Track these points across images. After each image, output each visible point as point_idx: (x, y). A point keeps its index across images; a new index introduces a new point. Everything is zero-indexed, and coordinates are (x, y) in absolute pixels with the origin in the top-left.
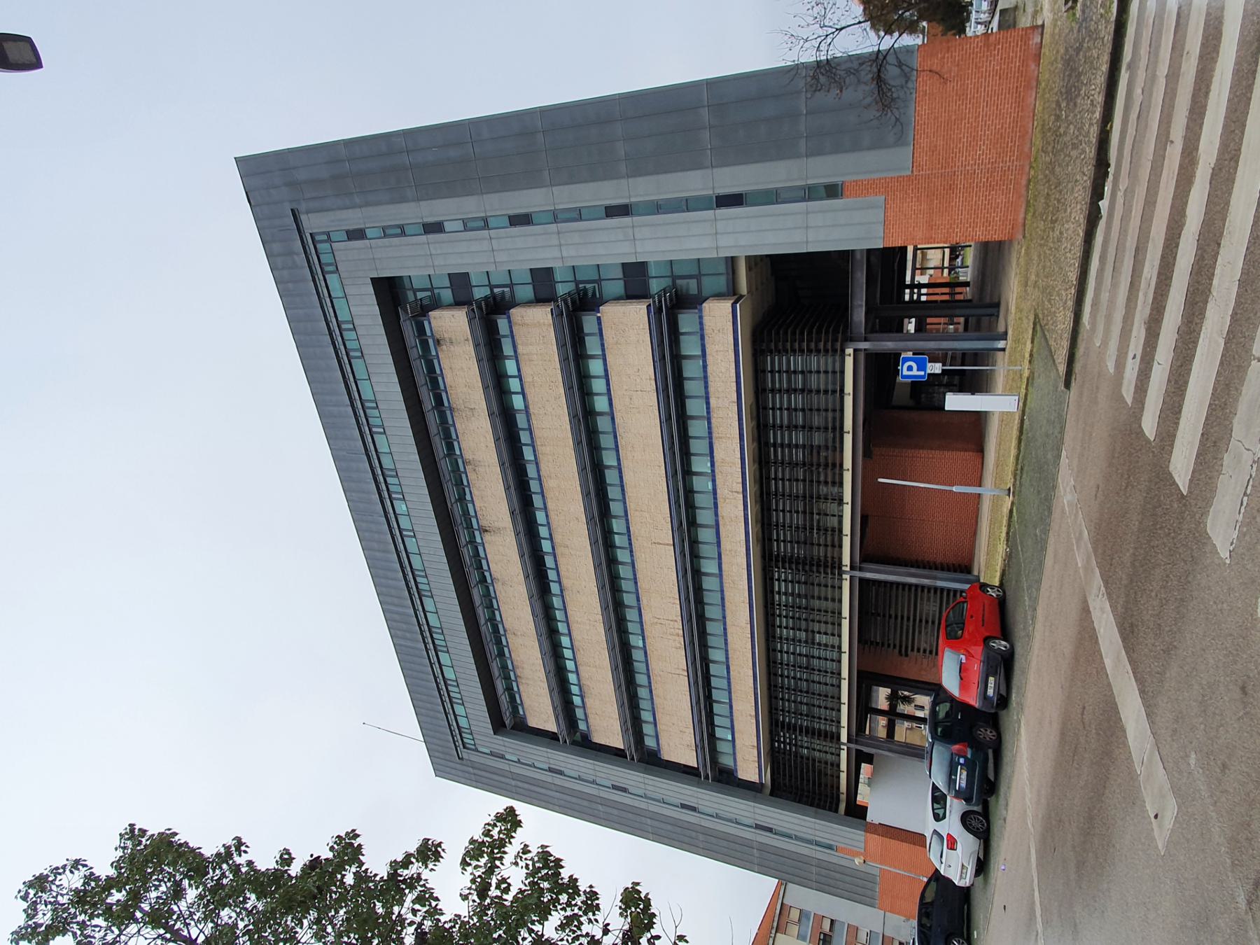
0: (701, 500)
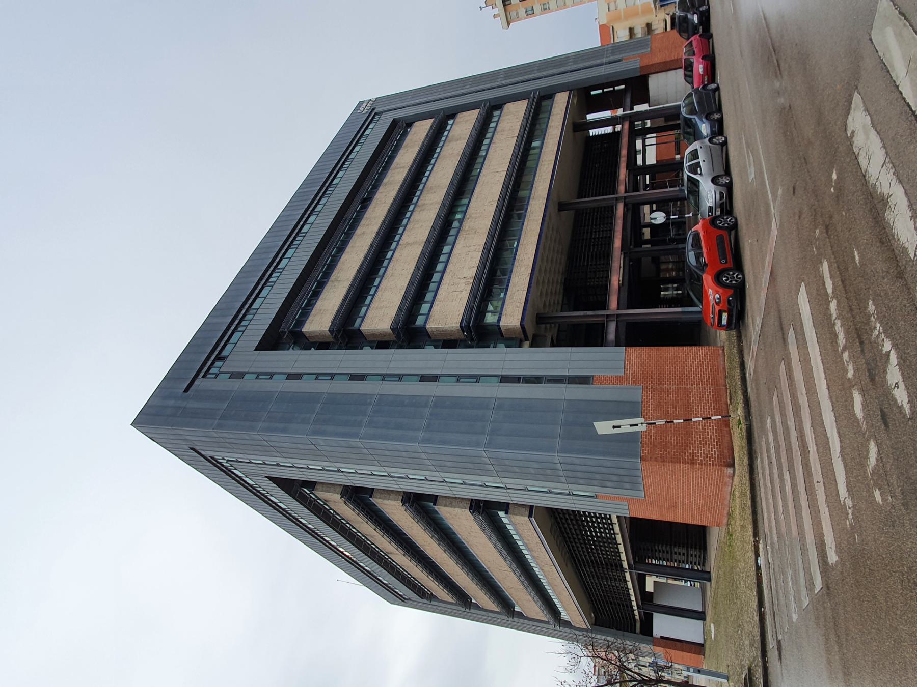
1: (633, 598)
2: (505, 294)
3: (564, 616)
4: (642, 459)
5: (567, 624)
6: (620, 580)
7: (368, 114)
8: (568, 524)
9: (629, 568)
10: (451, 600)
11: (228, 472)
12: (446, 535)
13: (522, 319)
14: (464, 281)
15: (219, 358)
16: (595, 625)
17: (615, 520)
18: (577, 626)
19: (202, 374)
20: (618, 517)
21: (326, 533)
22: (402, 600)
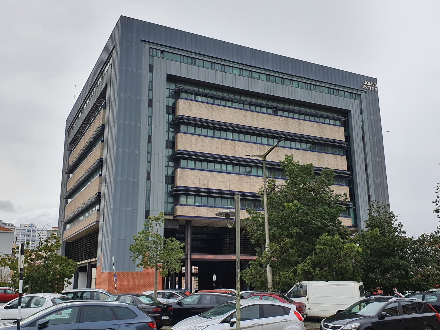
0: (259, 139)
1: (81, 263)
2: (198, 206)
3: (68, 226)
4: (109, 272)
5: (65, 229)
6: (89, 256)
7: (363, 89)
8: (94, 238)
9: (89, 263)
10: (70, 163)
11: (108, 61)
12: (92, 174)
13: (181, 216)
14: (206, 183)
15: (162, 52)
16: (66, 242)
17: (94, 259)
18: (64, 233)
19: (152, 46)
20: (96, 261)
21: (97, 89)
22: (68, 131)
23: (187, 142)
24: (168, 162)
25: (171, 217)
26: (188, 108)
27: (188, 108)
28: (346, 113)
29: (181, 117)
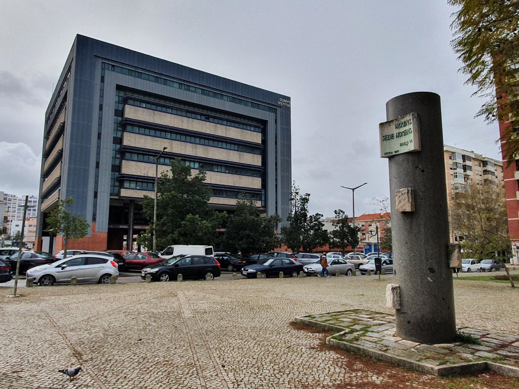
23: (131, 140)
24: (118, 127)
25: (117, 197)
26: (132, 112)
27: (132, 112)
28: (264, 123)
29: (127, 120)
